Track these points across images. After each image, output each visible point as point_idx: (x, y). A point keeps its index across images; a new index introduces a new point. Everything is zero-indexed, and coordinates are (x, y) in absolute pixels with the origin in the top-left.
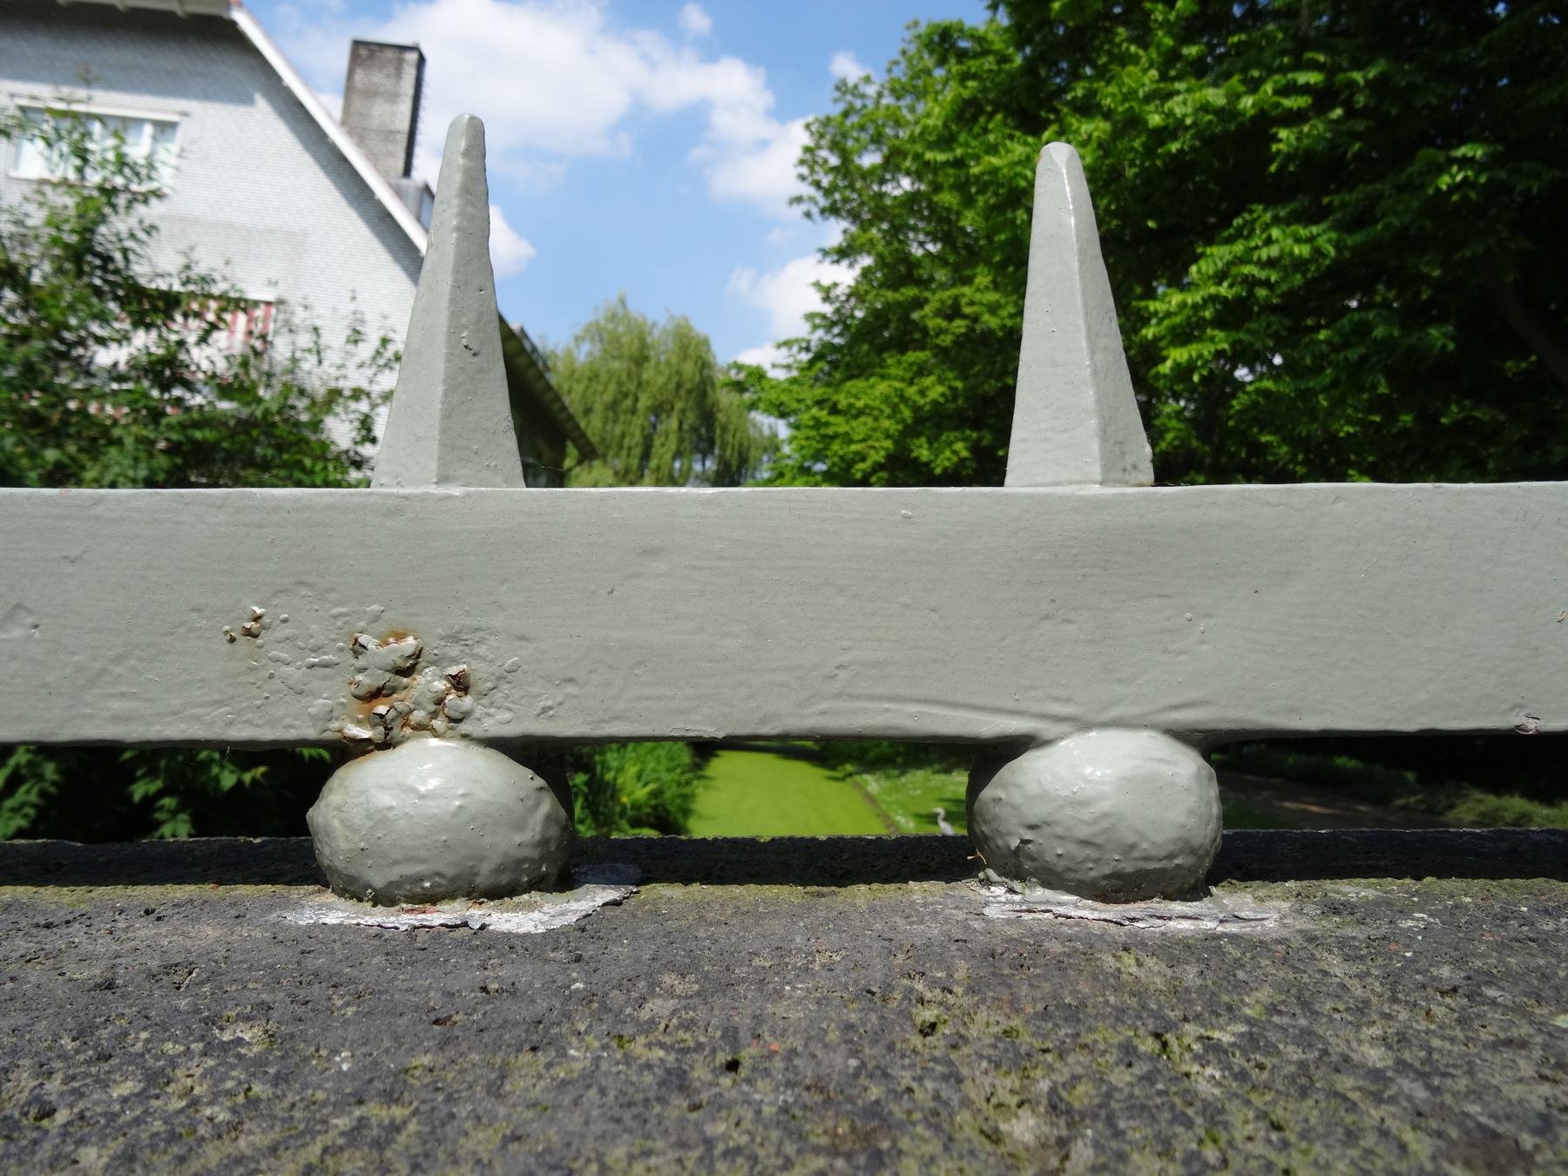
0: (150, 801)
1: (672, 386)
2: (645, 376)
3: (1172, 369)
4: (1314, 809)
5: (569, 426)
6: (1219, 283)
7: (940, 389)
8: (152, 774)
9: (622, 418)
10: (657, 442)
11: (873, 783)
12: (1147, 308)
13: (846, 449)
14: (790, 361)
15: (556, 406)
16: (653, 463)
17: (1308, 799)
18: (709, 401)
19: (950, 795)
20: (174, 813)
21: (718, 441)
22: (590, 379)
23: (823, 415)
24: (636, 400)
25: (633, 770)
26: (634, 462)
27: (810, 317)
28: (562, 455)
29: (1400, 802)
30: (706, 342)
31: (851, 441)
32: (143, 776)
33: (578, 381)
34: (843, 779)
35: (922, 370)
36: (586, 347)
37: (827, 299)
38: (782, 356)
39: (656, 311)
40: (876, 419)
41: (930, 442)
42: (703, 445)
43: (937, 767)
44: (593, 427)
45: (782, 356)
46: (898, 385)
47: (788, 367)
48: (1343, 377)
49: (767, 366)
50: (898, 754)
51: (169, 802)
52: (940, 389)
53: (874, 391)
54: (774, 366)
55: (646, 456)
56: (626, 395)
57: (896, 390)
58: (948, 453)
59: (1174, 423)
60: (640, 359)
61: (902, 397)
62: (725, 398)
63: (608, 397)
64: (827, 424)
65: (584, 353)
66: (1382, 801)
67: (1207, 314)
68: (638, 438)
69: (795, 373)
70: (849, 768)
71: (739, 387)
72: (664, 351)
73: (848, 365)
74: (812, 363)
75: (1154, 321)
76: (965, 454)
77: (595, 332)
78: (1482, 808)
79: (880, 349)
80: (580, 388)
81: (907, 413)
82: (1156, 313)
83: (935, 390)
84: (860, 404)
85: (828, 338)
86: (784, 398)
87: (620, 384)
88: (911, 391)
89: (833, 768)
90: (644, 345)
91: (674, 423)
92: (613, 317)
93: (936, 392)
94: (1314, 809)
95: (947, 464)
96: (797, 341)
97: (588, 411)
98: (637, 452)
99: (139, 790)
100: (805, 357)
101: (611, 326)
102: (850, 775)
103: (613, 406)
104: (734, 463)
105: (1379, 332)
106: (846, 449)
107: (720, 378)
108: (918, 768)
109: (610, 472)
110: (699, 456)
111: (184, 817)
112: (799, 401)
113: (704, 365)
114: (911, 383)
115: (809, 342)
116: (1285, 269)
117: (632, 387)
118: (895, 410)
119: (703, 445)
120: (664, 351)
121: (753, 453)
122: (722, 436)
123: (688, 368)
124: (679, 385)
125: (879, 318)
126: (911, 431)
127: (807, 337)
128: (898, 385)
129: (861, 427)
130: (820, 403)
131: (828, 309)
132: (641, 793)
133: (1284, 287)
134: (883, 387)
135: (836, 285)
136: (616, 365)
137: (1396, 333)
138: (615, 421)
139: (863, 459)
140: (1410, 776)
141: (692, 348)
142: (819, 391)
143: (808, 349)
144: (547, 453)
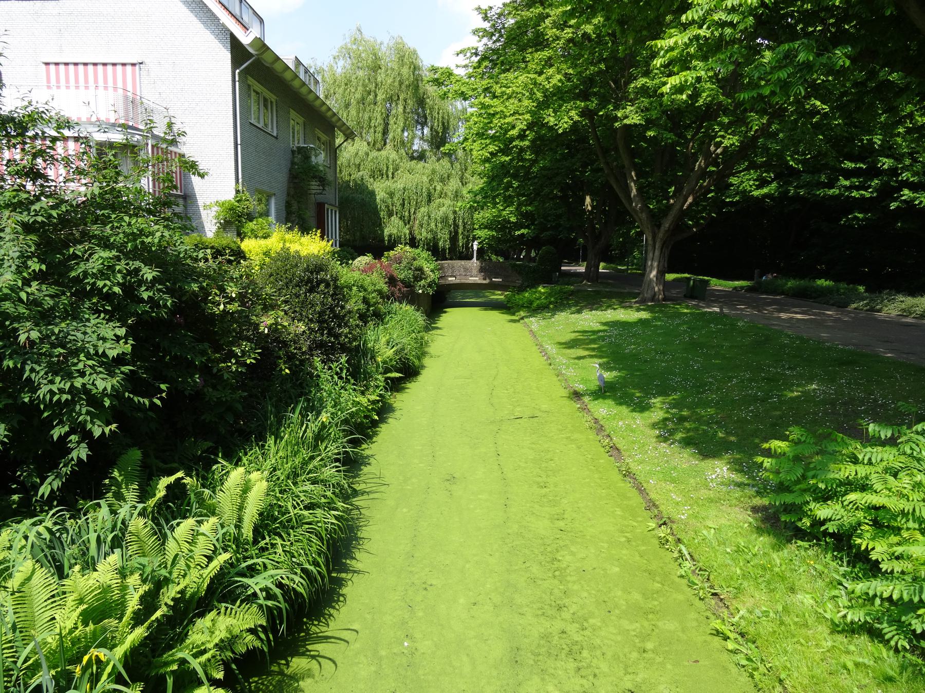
0: (63, 439)
1: (396, 84)
2: (379, 79)
3: (671, 89)
4: (799, 316)
5: (334, 119)
6: (701, 27)
7: (559, 77)
8: (61, 422)
9: (368, 109)
10: (392, 122)
11: (535, 322)
12: (656, 45)
13: (502, 121)
14: (467, 62)
15: (324, 108)
16: (391, 136)
17: (796, 310)
18: (421, 91)
19: (579, 328)
20: (79, 443)
21: (429, 118)
22: (346, 84)
23: (487, 101)
24: (376, 96)
25: (383, 340)
26: (379, 136)
27: (475, 32)
28: (333, 138)
29: (854, 306)
30: (415, 52)
31: (505, 117)
32: (57, 425)
33: (339, 87)
34: (518, 321)
35: (549, 63)
36: (341, 63)
37: (486, 18)
38: (462, 60)
39: (382, 35)
40: (520, 100)
41: (555, 112)
42: (422, 120)
43: (573, 309)
44: (349, 117)
45: (462, 60)
46: (533, 76)
47: (466, 66)
48: (778, 91)
49: (453, 67)
50: (551, 303)
51: (74, 438)
52: (559, 77)
53: (518, 80)
54: (457, 66)
55: (385, 132)
56: (369, 93)
57: (531, 79)
58: (566, 119)
59: (708, 85)
60: (376, 68)
61: (535, 84)
62: (432, 90)
63: (358, 96)
64: (490, 106)
65: (341, 67)
66: (842, 305)
67: (692, 50)
68: (380, 120)
69: (471, 70)
70: (522, 314)
71: (437, 82)
72: (389, 59)
73: (502, 63)
74: (480, 62)
75: (662, 53)
76: (576, 118)
77: (346, 53)
78: (903, 306)
79: (522, 49)
80: (341, 90)
81: (539, 95)
82: (662, 48)
83: (554, 78)
84: (509, 91)
85: (490, 44)
86: (464, 89)
87: (364, 86)
88: (540, 79)
89: (513, 314)
90: (376, 58)
91: (401, 109)
92: (355, 41)
93: (556, 79)
94: (799, 316)
95: (566, 126)
96: (469, 49)
97: (347, 106)
98: (380, 129)
99: (56, 433)
100: (475, 59)
101: (355, 47)
102: (522, 318)
103: (362, 101)
104: (440, 130)
105: (802, 57)
106: (502, 121)
107: (427, 75)
108: (562, 311)
109: (365, 143)
110: (419, 127)
111: (84, 445)
112: (474, 90)
113: (415, 68)
114: (540, 73)
115: (477, 49)
116: (743, 13)
117: (372, 87)
118: (532, 94)
119: (422, 120)
120: (389, 59)
121: (453, 122)
122: (431, 113)
123: (405, 71)
124: (401, 83)
125: (521, 26)
126: (543, 105)
127: (475, 45)
128: (533, 76)
129: (513, 104)
130: (487, 90)
131: (487, 25)
132: (390, 353)
133: (741, 27)
134: (523, 78)
135: (491, 8)
136: (361, 73)
137: (811, 59)
138: (364, 110)
139: (514, 127)
140: (861, 289)
141: (407, 58)
142: (485, 82)
143: (476, 54)
144: (324, 137)
